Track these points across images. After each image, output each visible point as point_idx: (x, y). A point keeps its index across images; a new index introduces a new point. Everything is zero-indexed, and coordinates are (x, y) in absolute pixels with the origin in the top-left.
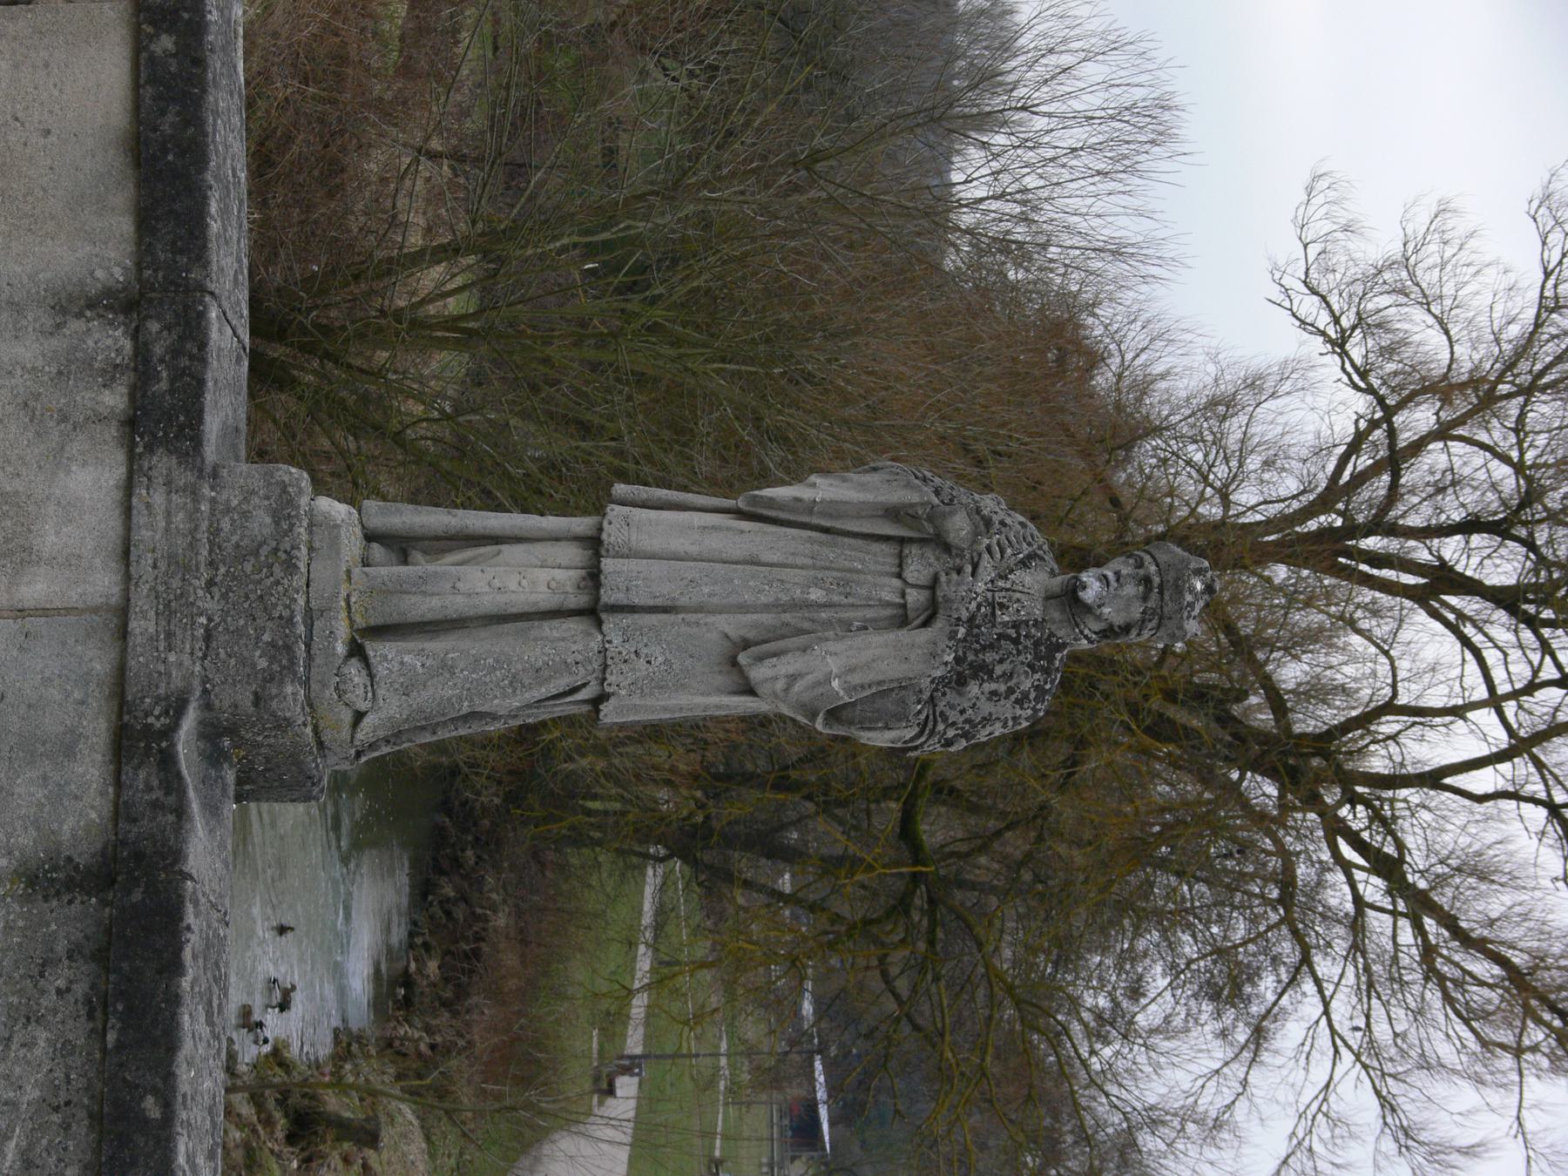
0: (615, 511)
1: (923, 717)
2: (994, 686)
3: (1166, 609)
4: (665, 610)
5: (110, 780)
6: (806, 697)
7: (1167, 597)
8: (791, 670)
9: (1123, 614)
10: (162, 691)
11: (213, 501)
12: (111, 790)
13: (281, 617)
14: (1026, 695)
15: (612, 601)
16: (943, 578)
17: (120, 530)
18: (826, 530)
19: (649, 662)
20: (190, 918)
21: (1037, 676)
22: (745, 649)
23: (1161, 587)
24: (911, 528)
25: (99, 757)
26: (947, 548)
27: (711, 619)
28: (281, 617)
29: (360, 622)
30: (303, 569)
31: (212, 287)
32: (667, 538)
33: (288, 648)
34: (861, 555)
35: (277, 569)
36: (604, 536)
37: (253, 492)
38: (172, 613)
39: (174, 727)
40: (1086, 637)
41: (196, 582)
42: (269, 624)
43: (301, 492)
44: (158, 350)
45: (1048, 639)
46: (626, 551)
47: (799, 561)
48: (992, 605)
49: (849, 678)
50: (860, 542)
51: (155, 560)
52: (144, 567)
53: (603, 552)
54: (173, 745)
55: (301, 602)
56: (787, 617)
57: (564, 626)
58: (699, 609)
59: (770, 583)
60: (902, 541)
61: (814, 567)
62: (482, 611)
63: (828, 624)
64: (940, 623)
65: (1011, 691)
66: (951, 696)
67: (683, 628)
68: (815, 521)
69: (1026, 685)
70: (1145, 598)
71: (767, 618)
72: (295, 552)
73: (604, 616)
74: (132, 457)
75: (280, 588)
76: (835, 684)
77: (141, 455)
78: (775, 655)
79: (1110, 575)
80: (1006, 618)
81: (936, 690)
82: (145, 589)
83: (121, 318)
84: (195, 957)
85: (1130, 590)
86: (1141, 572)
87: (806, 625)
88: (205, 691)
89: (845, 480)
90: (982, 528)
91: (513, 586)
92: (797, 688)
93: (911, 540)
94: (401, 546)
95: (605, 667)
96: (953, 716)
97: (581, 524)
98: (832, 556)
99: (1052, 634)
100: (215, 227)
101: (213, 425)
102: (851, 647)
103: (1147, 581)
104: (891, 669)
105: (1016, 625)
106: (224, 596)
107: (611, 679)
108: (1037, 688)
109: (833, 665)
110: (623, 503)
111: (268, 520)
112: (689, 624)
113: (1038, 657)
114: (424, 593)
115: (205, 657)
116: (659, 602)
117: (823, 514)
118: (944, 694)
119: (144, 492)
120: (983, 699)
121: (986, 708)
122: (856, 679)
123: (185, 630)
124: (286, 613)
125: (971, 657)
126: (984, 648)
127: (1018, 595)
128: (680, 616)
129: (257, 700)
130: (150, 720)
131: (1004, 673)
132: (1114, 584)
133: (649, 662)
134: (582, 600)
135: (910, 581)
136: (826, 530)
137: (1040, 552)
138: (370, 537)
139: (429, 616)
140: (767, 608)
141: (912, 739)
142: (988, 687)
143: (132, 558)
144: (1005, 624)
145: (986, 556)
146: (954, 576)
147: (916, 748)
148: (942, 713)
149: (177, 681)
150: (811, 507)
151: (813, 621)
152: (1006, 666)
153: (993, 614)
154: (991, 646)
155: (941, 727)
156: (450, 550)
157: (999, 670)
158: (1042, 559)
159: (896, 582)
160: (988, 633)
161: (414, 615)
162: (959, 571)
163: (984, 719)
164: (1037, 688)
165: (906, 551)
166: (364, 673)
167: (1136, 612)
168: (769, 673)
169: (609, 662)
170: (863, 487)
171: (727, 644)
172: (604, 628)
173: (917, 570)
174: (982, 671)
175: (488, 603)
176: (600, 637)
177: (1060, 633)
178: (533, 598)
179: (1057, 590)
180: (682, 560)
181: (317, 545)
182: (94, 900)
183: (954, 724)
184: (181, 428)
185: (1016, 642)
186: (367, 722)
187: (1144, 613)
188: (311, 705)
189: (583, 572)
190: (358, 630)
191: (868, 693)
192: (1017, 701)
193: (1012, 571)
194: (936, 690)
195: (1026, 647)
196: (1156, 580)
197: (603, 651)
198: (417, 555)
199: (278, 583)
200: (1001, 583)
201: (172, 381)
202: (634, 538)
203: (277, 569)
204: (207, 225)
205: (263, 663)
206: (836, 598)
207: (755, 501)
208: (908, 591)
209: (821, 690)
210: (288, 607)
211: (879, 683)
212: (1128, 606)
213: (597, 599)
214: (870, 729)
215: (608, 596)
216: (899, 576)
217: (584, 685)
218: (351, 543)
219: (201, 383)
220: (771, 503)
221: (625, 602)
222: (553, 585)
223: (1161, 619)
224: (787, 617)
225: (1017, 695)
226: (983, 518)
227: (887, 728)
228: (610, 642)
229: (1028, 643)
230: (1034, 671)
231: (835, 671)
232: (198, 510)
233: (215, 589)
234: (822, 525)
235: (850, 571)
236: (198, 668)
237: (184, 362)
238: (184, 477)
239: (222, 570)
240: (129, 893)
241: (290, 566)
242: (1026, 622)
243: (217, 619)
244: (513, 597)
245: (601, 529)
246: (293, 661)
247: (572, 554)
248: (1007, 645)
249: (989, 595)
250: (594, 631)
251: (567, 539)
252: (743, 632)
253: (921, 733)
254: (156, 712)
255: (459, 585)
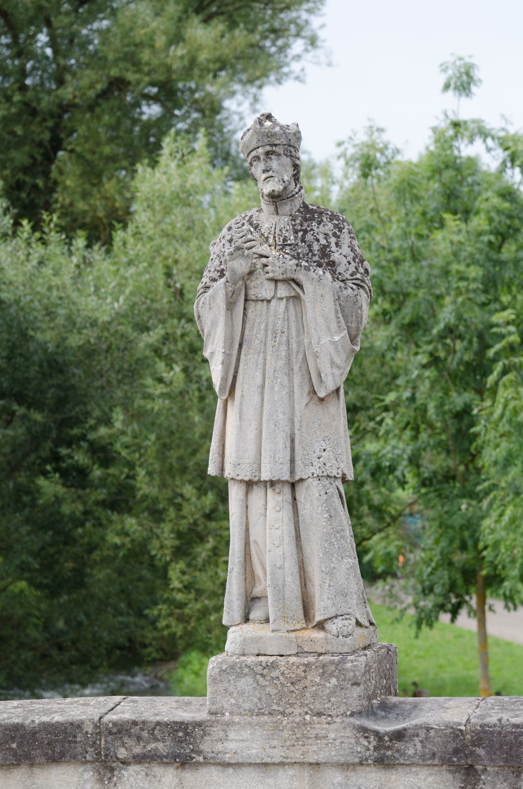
0: (228, 473)
1: (354, 287)
2: (333, 245)
3: (285, 143)
4: (293, 441)
5: (408, 769)
6: (344, 356)
7: (278, 142)
8: (329, 365)
9: (288, 168)
10: (353, 741)
11: (231, 713)
12: (414, 769)
13: (305, 671)
14: (336, 226)
15: (288, 473)
16: (271, 275)
17: (251, 769)
18: (241, 345)
19: (324, 450)
20: (493, 720)
21: (325, 220)
22: (315, 392)
23: (272, 145)
24: (239, 295)
25: (393, 777)
26: (251, 273)
27: (297, 414)
28: (305, 671)
29: (302, 624)
30: (274, 658)
31: (96, 719)
32: (241, 441)
33: (324, 666)
34: (256, 325)
35: (274, 674)
36: (247, 479)
37: (226, 690)
38: (304, 736)
39: (377, 733)
40: (300, 190)
41: (285, 723)
42: (309, 678)
43: (224, 661)
44: (138, 750)
45: (300, 212)
46: (256, 465)
47: (261, 361)
48: (284, 246)
49: (334, 330)
50: (248, 326)
51: (270, 747)
52: (277, 755)
53: (256, 479)
54: (386, 734)
55: (293, 659)
56: (296, 368)
57: (303, 500)
58: (292, 421)
59: (276, 378)
60: (246, 300)
61: (265, 352)
62: (295, 552)
63: (300, 343)
64: (301, 276)
65: (335, 235)
66: (340, 269)
67: (303, 429)
68: (235, 352)
69: (330, 226)
70: (279, 155)
71: (297, 380)
72: (264, 664)
73: (297, 478)
74: (207, 763)
75: (286, 672)
76: (337, 338)
77: (205, 758)
78: (320, 375)
79: (264, 176)
80: (292, 237)
81: (338, 278)
82: (291, 754)
83: (116, 773)
84: (517, 716)
85: (274, 164)
86: (262, 157)
87: (301, 356)
88: (352, 715)
89: (209, 335)
90: (240, 252)
91: (279, 532)
92: (339, 362)
93: (246, 295)
94: (251, 600)
95: (328, 476)
96: (352, 269)
97: (235, 494)
98: (257, 342)
99: (299, 211)
100: (57, 718)
101: (185, 715)
102: (315, 329)
103: (267, 153)
104: (328, 305)
105: (296, 232)
106: (292, 705)
107: (334, 473)
108: (331, 220)
109: (325, 340)
110: (222, 469)
111: (243, 680)
112: (301, 426)
113: (312, 219)
114: (284, 585)
115: (330, 716)
116: (288, 445)
117: (231, 347)
118: (340, 274)
119: (227, 755)
120: (340, 251)
121: (345, 249)
122: (334, 326)
123: (314, 728)
124: (302, 668)
125: (316, 258)
126: (311, 251)
127: (277, 231)
128: (297, 432)
129: (357, 684)
130: (371, 747)
131: (325, 238)
132: (270, 173)
133: (324, 450)
134: (287, 490)
135: (272, 295)
136: (241, 345)
137: (247, 218)
138: (246, 619)
139: (298, 582)
140: (291, 380)
141: (366, 293)
142: (334, 248)
143: (269, 760)
144: (296, 238)
145: (254, 250)
146: (268, 269)
147: (370, 291)
148: (352, 275)
149: (349, 732)
150: (227, 355)
151: (298, 352)
152: (321, 237)
153: (290, 245)
154: (310, 246)
155: (359, 276)
156: (253, 572)
157: (323, 242)
158: (251, 217)
159: (273, 303)
160: (303, 249)
161: (297, 592)
162: (265, 266)
163: (352, 250)
164: (331, 220)
165: (253, 298)
166: (335, 621)
167: (287, 161)
168: (330, 378)
169: (325, 474)
170: (214, 324)
171: (311, 405)
172: (304, 477)
173: (265, 290)
174: (325, 252)
175: (289, 547)
176: (310, 480)
177: (298, 206)
178: (286, 520)
179: (272, 208)
180: (261, 432)
181: (256, 652)
182: (483, 777)
183: (356, 268)
184: (187, 734)
185: (305, 232)
186: (361, 620)
187: (286, 155)
188: (354, 652)
189: (269, 491)
190: (307, 625)
191: (342, 319)
192: (340, 231)
193: (263, 235)
194: (338, 278)
195: (308, 226)
196: (268, 148)
197: (319, 478)
198: (257, 591)
199: (283, 674)
200: (271, 241)
201: (157, 740)
202: (247, 461)
203: (274, 674)
204: (57, 722)
205: (334, 681)
206: (284, 339)
207: (222, 388)
208: (279, 296)
209: (340, 347)
210: (298, 667)
211: (336, 312)
212: (283, 165)
213: (287, 482)
214: (362, 318)
215: (286, 477)
216: (269, 301)
217: (338, 489)
218: (250, 630)
219: (158, 723)
220: (224, 379)
221: (289, 465)
222: (278, 508)
223: (290, 146)
224: (296, 368)
225: (336, 231)
226: (235, 251)
227: (361, 308)
228: (313, 474)
229: (306, 224)
230: (322, 221)
231: (329, 339)
232: (238, 723)
233: (287, 711)
234: (238, 346)
235: (266, 330)
236: (338, 720)
237: (145, 734)
238: (217, 732)
239: (275, 707)
240: (480, 756)
241: (273, 666)
242: (294, 226)
243: (306, 709)
244: (286, 532)
245: (241, 481)
246: (332, 662)
247: (257, 496)
248: (309, 237)
249: (278, 247)
250: (306, 484)
251: (247, 500)
252: (305, 394)
253: (362, 287)
254: (366, 743)
255: (278, 565)
